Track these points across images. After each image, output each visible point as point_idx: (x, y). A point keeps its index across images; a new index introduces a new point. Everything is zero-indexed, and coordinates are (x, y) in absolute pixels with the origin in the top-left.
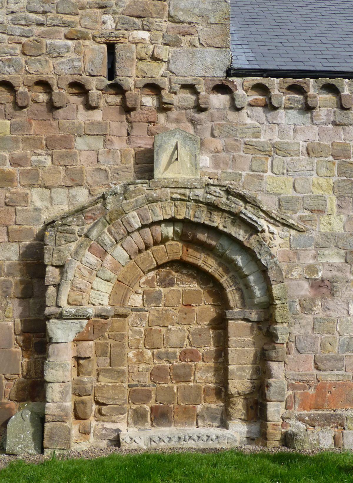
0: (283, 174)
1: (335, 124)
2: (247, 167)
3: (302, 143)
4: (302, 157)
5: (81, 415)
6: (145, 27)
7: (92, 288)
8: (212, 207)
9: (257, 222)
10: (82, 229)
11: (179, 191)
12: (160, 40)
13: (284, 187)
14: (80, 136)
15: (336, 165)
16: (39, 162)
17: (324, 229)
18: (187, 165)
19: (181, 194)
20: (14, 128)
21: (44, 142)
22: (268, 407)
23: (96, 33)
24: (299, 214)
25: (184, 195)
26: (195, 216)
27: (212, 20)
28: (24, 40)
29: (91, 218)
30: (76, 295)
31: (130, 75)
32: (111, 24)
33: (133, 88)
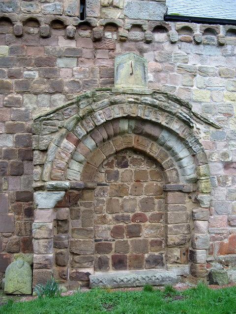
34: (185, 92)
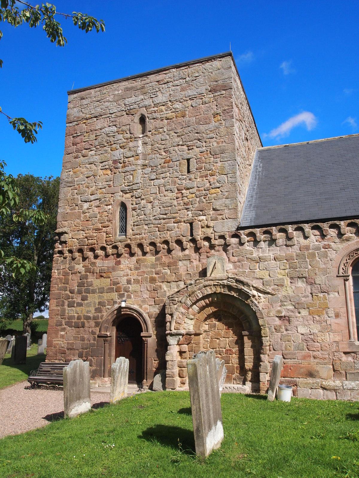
0: (264, 270)
1: (286, 245)
2: (248, 268)
3: (272, 255)
4: (272, 261)
5: (181, 376)
6: (204, 214)
7: (185, 323)
8: (230, 288)
9: (249, 293)
10: (179, 299)
12: (210, 219)
13: (265, 276)
14: (180, 260)
15: (288, 264)
16: (165, 272)
17: (284, 293)
18: (223, 269)
19: (217, 282)
20: (157, 259)
21: (167, 264)
22: (260, 375)
23: (185, 219)
24: (272, 287)
26: (224, 292)
27: (230, 208)
28: (159, 226)
29: (182, 295)
30: (177, 326)
31: (198, 234)
32: (190, 215)
33: (199, 239)
34: (252, 273)
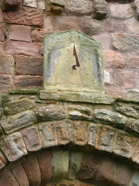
11: (79, 107)
25: (87, 112)
